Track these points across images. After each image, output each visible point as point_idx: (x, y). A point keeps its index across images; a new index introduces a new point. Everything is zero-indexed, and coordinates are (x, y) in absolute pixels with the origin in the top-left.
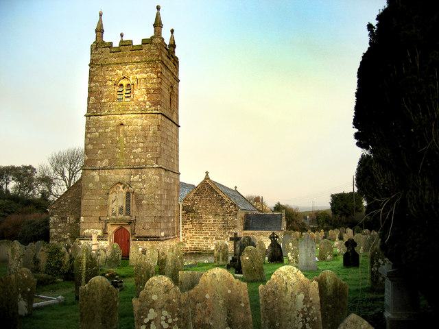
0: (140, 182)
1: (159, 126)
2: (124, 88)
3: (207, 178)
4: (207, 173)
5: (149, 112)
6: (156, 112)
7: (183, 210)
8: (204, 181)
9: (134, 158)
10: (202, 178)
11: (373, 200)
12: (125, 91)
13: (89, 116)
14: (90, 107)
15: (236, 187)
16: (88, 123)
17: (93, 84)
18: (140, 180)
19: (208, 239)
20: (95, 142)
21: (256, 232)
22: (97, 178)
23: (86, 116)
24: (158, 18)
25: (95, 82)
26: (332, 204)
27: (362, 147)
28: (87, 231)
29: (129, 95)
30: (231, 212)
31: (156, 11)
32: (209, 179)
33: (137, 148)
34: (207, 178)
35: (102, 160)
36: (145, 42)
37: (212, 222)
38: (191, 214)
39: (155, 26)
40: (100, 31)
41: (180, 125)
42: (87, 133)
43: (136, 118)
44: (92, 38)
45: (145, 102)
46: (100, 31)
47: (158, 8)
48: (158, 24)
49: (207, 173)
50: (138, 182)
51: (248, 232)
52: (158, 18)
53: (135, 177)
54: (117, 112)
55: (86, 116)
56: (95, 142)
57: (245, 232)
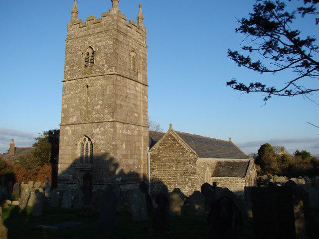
1: (114, 85)
4: (171, 125)
5: (106, 74)
6: (112, 73)
7: (150, 159)
9: (96, 114)
11: (73, 131)
15: (230, 139)
18: (99, 132)
20: (68, 102)
21: (223, 178)
22: (70, 132)
26: (302, 41)
30: (190, 160)
33: (97, 105)
35: (72, 116)
38: (158, 162)
41: (148, 84)
42: (63, 95)
43: (96, 80)
45: (103, 65)
49: (171, 125)
51: (216, 178)
54: (83, 77)
56: (68, 102)
57: (214, 178)
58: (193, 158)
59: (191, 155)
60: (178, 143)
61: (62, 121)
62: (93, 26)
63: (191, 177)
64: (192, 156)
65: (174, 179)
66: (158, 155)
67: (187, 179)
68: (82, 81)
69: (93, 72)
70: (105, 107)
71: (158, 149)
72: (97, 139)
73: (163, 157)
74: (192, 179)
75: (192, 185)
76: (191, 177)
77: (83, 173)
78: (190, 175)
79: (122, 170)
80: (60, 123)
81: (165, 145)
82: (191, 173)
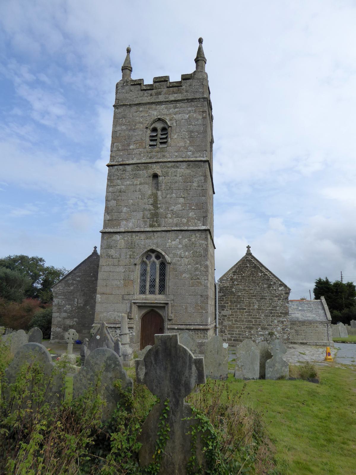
0: (179, 249)
2: (159, 132)
3: (249, 254)
8: (245, 257)
10: (243, 253)
12: (160, 136)
13: (112, 166)
14: (114, 154)
16: (109, 175)
17: (118, 128)
19: (251, 328)
23: (108, 166)
24: (200, 51)
25: (121, 125)
27: (149, 350)
28: (105, 314)
29: (165, 141)
30: (280, 295)
31: (198, 44)
32: (251, 254)
33: (176, 204)
34: (249, 254)
36: (185, 78)
37: (256, 307)
39: (197, 61)
40: (127, 68)
44: (119, 77)
45: (186, 148)
46: (127, 68)
47: (200, 41)
48: (200, 59)
49: (248, 247)
50: (176, 248)
52: (200, 51)
53: (174, 243)
55: (108, 166)
58: (283, 292)
59: (280, 289)
60: (262, 272)
61: (105, 226)
62: (165, 90)
63: (281, 319)
64: (282, 290)
65: (256, 321)
66: (232, 287)
67: (276, 321)
68: (146, 168)
69: (168, 155)
70: (190, 208)
71: (231, 279)
72: (175, 255)
73: (240, 290)
74: (282, 322)
75: (283, 329)
76: (281, 319)
77: (144, 311)
78: (280, 316)
79: (27, 333)
80: (101, 228)
81: (241, 274)
82: (281, 313)
